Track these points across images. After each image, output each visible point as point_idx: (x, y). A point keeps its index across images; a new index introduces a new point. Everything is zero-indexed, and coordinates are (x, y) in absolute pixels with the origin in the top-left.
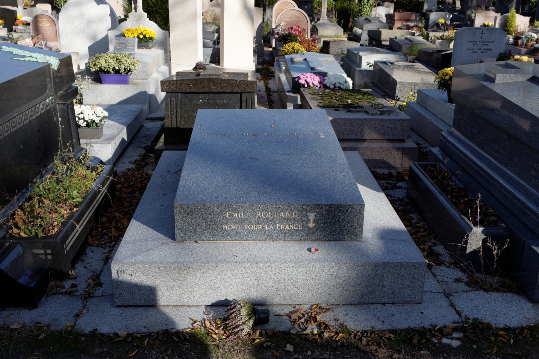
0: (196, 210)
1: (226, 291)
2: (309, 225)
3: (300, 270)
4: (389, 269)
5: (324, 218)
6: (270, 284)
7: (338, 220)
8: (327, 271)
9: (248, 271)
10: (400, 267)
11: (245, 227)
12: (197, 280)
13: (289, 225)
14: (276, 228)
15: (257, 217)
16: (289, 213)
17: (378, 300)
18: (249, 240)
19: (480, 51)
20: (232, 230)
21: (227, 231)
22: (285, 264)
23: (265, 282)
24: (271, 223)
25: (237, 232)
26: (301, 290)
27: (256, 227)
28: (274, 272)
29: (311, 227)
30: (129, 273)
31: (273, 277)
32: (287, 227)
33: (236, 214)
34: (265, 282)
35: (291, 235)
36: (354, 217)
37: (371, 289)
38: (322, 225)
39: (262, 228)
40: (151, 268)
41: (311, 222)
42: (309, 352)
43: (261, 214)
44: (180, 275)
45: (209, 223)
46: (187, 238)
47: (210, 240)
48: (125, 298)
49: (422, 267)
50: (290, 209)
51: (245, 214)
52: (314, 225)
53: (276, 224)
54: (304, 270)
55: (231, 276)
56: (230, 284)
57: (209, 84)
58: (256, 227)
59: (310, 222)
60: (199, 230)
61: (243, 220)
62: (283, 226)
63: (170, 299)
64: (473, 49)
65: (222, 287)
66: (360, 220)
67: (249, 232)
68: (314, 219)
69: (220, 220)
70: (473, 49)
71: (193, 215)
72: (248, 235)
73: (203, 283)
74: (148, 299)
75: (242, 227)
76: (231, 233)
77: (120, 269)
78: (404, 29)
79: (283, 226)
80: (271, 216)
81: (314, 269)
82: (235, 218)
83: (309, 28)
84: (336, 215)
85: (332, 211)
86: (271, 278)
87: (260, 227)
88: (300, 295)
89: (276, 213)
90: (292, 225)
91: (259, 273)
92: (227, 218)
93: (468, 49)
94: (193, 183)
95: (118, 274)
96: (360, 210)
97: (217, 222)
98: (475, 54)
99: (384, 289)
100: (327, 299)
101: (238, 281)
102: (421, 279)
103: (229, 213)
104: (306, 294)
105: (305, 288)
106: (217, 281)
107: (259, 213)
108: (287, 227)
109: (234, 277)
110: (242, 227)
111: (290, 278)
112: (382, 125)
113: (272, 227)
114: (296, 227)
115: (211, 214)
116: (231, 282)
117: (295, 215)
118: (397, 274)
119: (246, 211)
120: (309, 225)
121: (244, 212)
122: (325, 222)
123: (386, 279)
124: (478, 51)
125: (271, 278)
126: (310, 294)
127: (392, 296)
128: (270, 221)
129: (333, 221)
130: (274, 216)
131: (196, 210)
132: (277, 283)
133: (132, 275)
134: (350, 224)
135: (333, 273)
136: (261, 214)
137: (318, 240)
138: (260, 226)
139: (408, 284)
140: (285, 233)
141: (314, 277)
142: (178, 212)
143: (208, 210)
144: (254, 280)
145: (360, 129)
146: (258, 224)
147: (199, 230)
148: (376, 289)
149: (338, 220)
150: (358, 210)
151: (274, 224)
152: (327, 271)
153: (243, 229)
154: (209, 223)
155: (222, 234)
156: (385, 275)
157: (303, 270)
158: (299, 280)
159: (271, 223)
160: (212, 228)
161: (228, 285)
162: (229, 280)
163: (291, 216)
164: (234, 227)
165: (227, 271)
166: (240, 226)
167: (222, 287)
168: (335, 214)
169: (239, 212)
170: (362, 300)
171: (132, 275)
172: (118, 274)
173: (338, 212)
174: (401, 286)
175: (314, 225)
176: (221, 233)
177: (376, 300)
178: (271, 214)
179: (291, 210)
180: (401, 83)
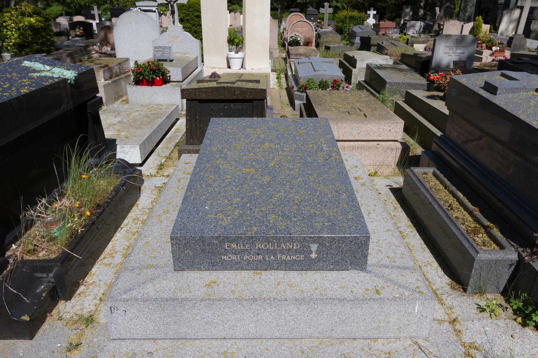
0: (194, 242)
1: (225, 326)
2: (311, 255)
3: (302, 308)
4: (396, 306)
5: (327, 249)
6: (270, 320)
7: (342, 251)
8: (329, 308)
9: (247, 308)
10: (407, 305)
11: (245, 258)
12: (194, 316)
13: (290, 256)
14: (277, 258)
15: (257, 248)
16: (290, 244)
17: (382, 335)
18: (249, 270)
19: (454, 54)
20: (231, 261)
21: (226, 261)
22: (286, 302)
23: (264, 318)
24: (272, 254)
25: (236, 262)
26: (302, 325)
27: (256, 258)
28: (274, 309)
29: (313, 258)
30: (122, 310)
31: (273, 314)
32: (289, 258)
33: (235, 246)
34: (264, 318)
35: (292, 265)
36: (359, 248)
37: (376, 325)
38: (325, 256)
39: (263, 258)
40: (145, 305)
41: (314, 253)
42: (316, 246)
43: (261, 245)
44: (176, 312)
45: (207, 254)
46: (185, 268)
47: (209, 270)
48: (121, 332)
49: (431, 305)
50: (291, 241)
51: (244, 246)
52: (316, 255)
53: (277, 255)
54: (306, 307)
55: (229, 313)
56: (228, 320)
57: (224, 92)
58: (256, 258)
59: (312, 253)
60: (197, 260)
61: (243, 251)
62: (284, 257)
63: (167, 333)
64: (449, 53)
65: (220, 322)
66: (365, 251)
67: (249, 262)
68: (317, 251)
69: (218, 251)
70: (449, 53)
71: (190, 246)
72: (248, 265)
73: (200, 319)
74: (144, 333)
75: (242, 258)
76: (231, 264)
77: (112, 306)
78: (495, 70)
79: (284, 257)
80: (272, 247)
81: (316, 307)
82: (234, 249)
83: (315, 35)
84: (339, 247)
85: (335, 242)
86: (271, 314)
87: (260, 257)
88: (301, 330)
89: (277, 244)
90: (293, 256)
91: (258, 310)
92: (226, 249)
93: (445, 53)
94: (194, 207)
95: (111, 310)
96: (365, 241)
97: (215, 253)
98: (450, 57)
99: (390, 325)
100: (330, 334)
101: (236, 317)
102: (429, 316)
103: (227, 244)
104: (308, 329)
105: (307, 324)
106: (214, 317)
107: (258, 245)
108: (289, 258)
109: (232, 313)
110: (242, 258)
111: (291, 314)
112: (378, 128)
113: (272, 257)
114: (297, 258)
115: (209, 245)
116: (229, 318)
117: (297, 246)
118: (404, 312)
119: (245, 243)
120: (311, 255)
121: (243, 243)
122: (327, 252)
123: (392, 316)
124: (453, 55)
125: (271, 314)
126: (311, 330)
127: (398, 331)
128: (270, 252)
129: (337, 252)
130: (274, 247)
131: (194, 242)
132: (277, 319)
133: (125, 312)
134: (354, 255)
135: (336, 311)
136: (261, 245)
137: (320, 270)
138: (260, 257)
139: (415, 321)
140: (287, 263)
141: (316, 313)
142: (174, 243)
143: (206, 242)
144: (253, 316)
145: (358, 131)
146: (258, 255)
147: (197, 260)
148: (381, 325)
149: (342, 251)
150: (363, 242)
151: (275, 254)
152: (329, 308)
153: (243, 259)
154: (207, 254)
155: (221, 264)
156: (391, 312)
157: (304, 307)
158: (301, 317)
159: (272, 254)
160: (211, 259)
161: (226, 321)
162: (226, 316)
163: (293, 247)
164: (234, 257)
165: (224, 308)
166: (240, 257)
167: (220, 322)
168: (339, 245)
169: (238, 243)
170: (365, 335)
171: (125, 312)
172: (111, 310)
173: (342, 244)
174: (407, 323)
175: (316, 255)
176: (220, 263)
177: (381, 335)
178: (271, 245)
179: (292, 242)
180: (391, 84)
